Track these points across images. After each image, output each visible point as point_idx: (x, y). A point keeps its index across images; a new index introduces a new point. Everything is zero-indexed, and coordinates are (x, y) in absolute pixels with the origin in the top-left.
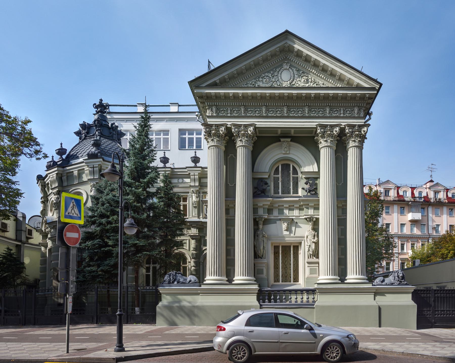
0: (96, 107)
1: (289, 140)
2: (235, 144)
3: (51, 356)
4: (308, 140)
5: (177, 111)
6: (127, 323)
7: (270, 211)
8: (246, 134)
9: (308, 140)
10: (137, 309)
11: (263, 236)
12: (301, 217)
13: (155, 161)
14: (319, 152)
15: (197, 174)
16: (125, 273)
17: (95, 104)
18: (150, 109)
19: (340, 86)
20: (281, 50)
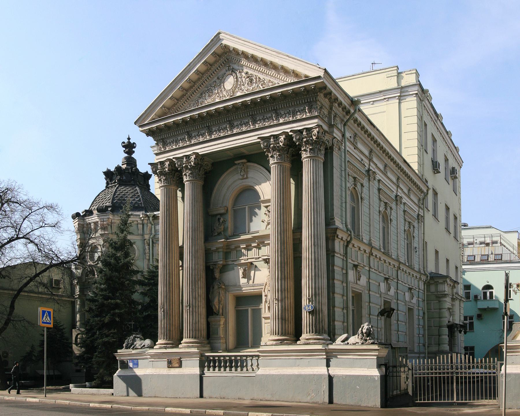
1: (244, 161)
2: (300, 156)
7: (227, 254)
8: (311, 140)
11: (219, 288)
16: (149, 357)
17: (124, 143)
19: (292, 81)
20: (221, 60)
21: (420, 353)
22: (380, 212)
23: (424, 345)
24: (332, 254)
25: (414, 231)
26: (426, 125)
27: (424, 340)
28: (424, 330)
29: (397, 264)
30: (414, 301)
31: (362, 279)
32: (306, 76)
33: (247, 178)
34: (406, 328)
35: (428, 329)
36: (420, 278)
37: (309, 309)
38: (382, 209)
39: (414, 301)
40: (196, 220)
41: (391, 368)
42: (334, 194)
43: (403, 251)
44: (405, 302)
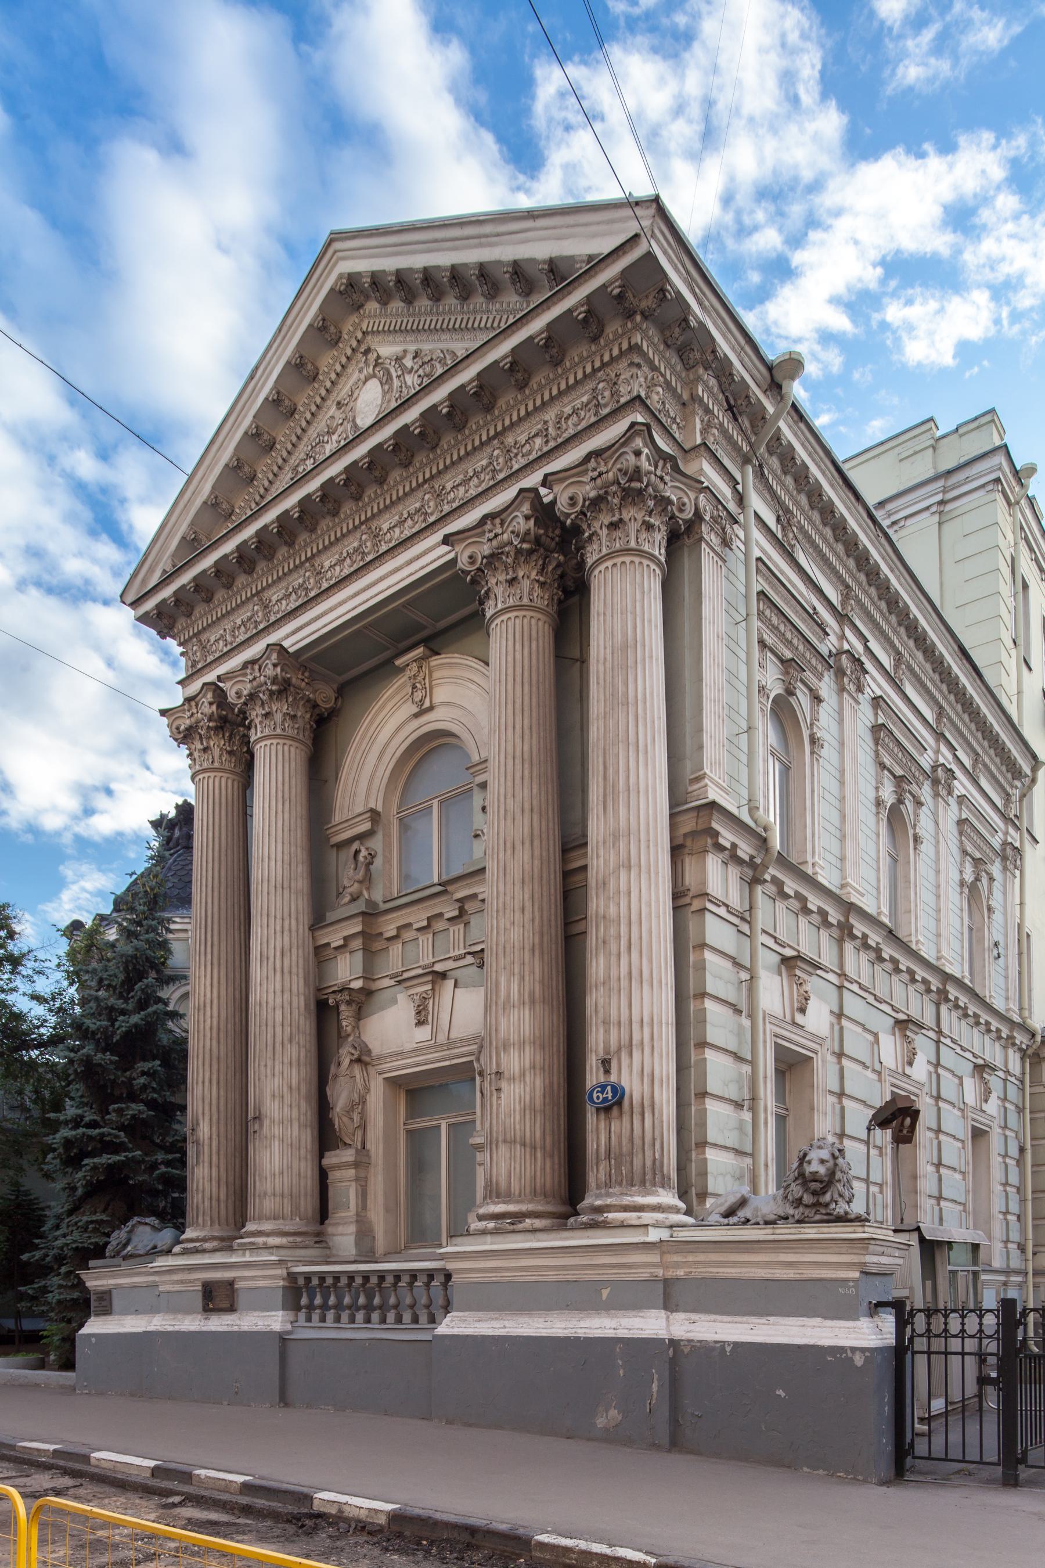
21: (1007, 1272)
22: (879, 803)
23: (1022, 1248)
24: (696, 905)
25: (990, 892)
26: (1025, 586)
27: (1023, 1231)
28: (1023, 1201)
29: (935, 984)
30: (992, 1106)
31: (813, 1005)
32: (590, 258)
33: (431, 708)
34: (967, 1192)
35: (1033, 1199)
36: (1011, 1038)
37: (605, 1100)
38: (888, 795)
39: (992, 1106)
40: (286, 858)
41: (920, 1321)
42: (706, 692)
43: (955, 945)
44: (963, 1109)
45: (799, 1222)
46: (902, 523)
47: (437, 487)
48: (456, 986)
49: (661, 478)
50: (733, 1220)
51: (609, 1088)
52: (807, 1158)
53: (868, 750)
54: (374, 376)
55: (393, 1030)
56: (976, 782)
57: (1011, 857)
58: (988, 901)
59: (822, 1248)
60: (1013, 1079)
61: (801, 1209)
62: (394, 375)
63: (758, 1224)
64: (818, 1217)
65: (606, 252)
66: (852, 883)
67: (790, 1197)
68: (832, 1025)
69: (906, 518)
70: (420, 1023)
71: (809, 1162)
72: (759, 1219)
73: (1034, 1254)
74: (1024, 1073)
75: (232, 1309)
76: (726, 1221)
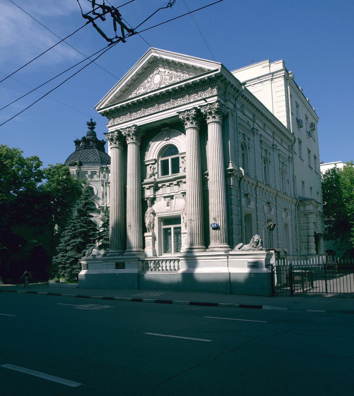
0: (89, 124)
1: (168, 128)
3: (245, 157)
4: (175, 126)
5: (269, 72)
6: (122, 41)
9: (175, 126)
10: (308, 271)
12: (98, 217)
13: (42, 166)
14: (127, 146)
15: (75, 171)
18: (227, 260)
23: (297, 250)
37: (215, 226)
45: (253, 250)
46: (263, 82)
47: (287, 271)
48: (176, 198)
49: (222, 108)
50: (241, 250)
51: (215, 224)
52: (254, 238)
53: (259, 146)
54: (159, 74)
55: (160, 207)
56: (282, 145)
57: (290, 159)
58: (286, 171)
59: (138, 161)
60: (293, 211)
61: (254, 248)
62: (163, 75)
63: (245, 251)
64: (257, 249)
65: (213, 70)
66: (258, 176)
67: (251, 246)
68: (255, 206)
69: (264, 81)
70: (168, 206)
71: (255, 239)
72: (246, 250)
73: (300, 251)
74: (295, 209)
75: (124, 268)
76: (239, 250)
